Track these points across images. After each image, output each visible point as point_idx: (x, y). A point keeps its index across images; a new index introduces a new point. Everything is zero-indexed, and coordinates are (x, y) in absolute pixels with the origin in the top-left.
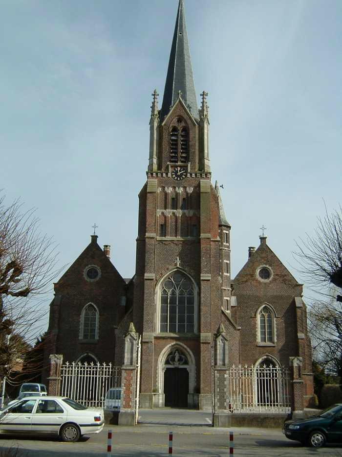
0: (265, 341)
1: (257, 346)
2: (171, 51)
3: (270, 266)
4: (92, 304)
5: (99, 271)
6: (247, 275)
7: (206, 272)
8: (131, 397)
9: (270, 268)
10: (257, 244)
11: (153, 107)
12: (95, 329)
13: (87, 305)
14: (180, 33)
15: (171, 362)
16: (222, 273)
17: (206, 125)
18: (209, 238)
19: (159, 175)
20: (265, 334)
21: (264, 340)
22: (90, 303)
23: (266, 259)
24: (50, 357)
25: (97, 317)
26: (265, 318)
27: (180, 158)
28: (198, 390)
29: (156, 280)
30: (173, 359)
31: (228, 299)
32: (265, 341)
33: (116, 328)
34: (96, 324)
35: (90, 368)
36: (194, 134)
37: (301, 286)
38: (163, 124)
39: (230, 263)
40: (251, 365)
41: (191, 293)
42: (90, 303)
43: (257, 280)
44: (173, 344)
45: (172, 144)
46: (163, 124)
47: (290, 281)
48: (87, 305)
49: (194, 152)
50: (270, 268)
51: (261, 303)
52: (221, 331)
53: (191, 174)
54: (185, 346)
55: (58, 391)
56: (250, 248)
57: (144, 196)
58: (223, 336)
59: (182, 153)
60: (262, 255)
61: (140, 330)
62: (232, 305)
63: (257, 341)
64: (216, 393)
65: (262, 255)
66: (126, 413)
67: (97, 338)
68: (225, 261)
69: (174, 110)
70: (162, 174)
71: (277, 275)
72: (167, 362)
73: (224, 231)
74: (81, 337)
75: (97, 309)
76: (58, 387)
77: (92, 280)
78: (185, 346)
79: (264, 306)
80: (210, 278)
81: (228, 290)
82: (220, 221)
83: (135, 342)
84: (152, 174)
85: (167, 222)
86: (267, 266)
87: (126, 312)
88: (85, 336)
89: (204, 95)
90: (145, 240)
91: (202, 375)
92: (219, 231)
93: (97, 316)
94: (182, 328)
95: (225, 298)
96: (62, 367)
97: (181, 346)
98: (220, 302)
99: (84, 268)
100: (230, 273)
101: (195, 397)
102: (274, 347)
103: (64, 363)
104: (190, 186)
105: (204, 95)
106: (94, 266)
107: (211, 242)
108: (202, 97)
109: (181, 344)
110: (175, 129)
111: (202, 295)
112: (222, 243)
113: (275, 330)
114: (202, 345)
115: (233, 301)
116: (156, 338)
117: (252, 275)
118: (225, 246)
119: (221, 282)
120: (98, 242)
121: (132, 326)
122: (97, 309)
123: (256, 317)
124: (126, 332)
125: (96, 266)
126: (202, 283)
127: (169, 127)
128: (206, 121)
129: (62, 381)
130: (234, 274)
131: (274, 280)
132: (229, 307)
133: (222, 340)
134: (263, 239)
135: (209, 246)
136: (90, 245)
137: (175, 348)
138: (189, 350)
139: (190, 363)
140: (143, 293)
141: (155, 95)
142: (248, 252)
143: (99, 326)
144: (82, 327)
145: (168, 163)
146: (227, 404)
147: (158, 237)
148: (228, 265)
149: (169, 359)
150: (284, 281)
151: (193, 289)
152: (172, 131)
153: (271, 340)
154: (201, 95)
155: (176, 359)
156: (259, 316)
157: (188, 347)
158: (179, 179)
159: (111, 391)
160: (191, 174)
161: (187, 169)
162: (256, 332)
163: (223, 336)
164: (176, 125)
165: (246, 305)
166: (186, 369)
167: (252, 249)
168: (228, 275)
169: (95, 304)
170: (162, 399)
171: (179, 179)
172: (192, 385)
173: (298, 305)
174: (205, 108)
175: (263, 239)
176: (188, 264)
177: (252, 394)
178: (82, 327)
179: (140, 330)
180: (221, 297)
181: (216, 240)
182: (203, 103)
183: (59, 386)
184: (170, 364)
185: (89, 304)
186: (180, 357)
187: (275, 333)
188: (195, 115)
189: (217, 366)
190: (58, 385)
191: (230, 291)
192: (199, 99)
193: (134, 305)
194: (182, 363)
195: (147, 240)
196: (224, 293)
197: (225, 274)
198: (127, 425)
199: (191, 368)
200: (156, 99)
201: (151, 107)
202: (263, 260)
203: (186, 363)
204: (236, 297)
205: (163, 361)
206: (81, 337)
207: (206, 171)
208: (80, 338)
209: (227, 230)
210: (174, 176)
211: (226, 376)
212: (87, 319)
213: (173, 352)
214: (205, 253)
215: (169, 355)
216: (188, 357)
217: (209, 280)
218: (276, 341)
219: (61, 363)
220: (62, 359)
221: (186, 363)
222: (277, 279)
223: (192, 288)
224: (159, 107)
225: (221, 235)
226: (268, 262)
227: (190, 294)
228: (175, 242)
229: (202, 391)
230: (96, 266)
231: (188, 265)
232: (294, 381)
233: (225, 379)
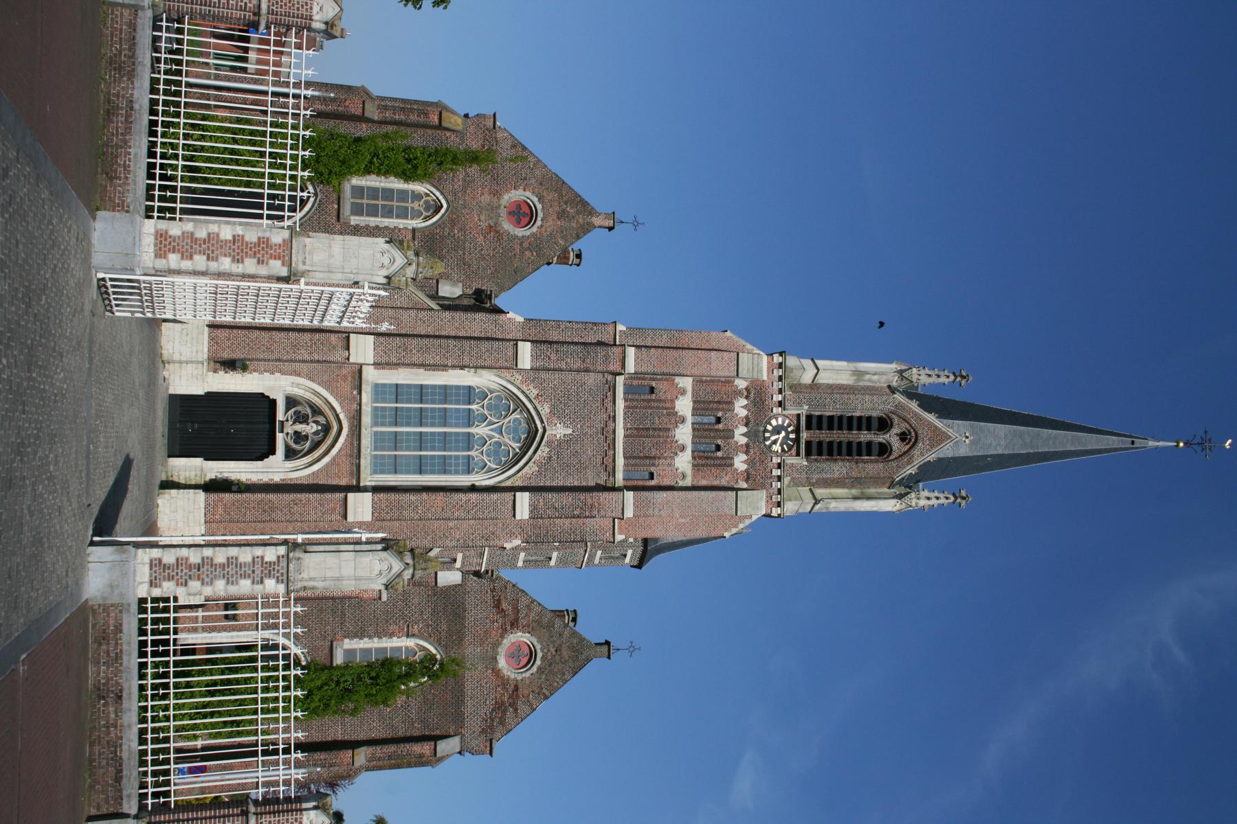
3: (539, 668)
4: (443, 211)
6: (516, 610)
7: (533, 508)
9: (535, 669)
10: (590, 630)
12: (377, 216)
13: (441, 198)
15: (293, 410)
22: (445, 206)
30: (301, 419)
31: (458, 564)
35: (293, 168)
40: (303, 627)
42: (445, 206)
43: (502, 637)
47: (502, 722)
48: (441, 198)
63: (346, 641)
69: (930, 424)
71: (516, 688)
72: (291, 402)
80: (518, 517)
86: (538, 662)
95: (460, 557)
98: (454, 543)
109: (342, 440)
122: (428, 223)
123: (408, 636)
136: (116, 522)
149: (299, 408)
150: (500, 707)
155: (299, 427)
162: (370, 637)
166: (274, 453)
168: (520, 564)
173: (442, 746)
177: (204, 629)
184: (287, 410)
185: (443, 202)
186: (306, 437)
196: (472, 552)
199: (275, 468)
202: (553, 650)
203: (290, 454)
222: (505, 688)
223: (491, 470)
228: (611, 423)
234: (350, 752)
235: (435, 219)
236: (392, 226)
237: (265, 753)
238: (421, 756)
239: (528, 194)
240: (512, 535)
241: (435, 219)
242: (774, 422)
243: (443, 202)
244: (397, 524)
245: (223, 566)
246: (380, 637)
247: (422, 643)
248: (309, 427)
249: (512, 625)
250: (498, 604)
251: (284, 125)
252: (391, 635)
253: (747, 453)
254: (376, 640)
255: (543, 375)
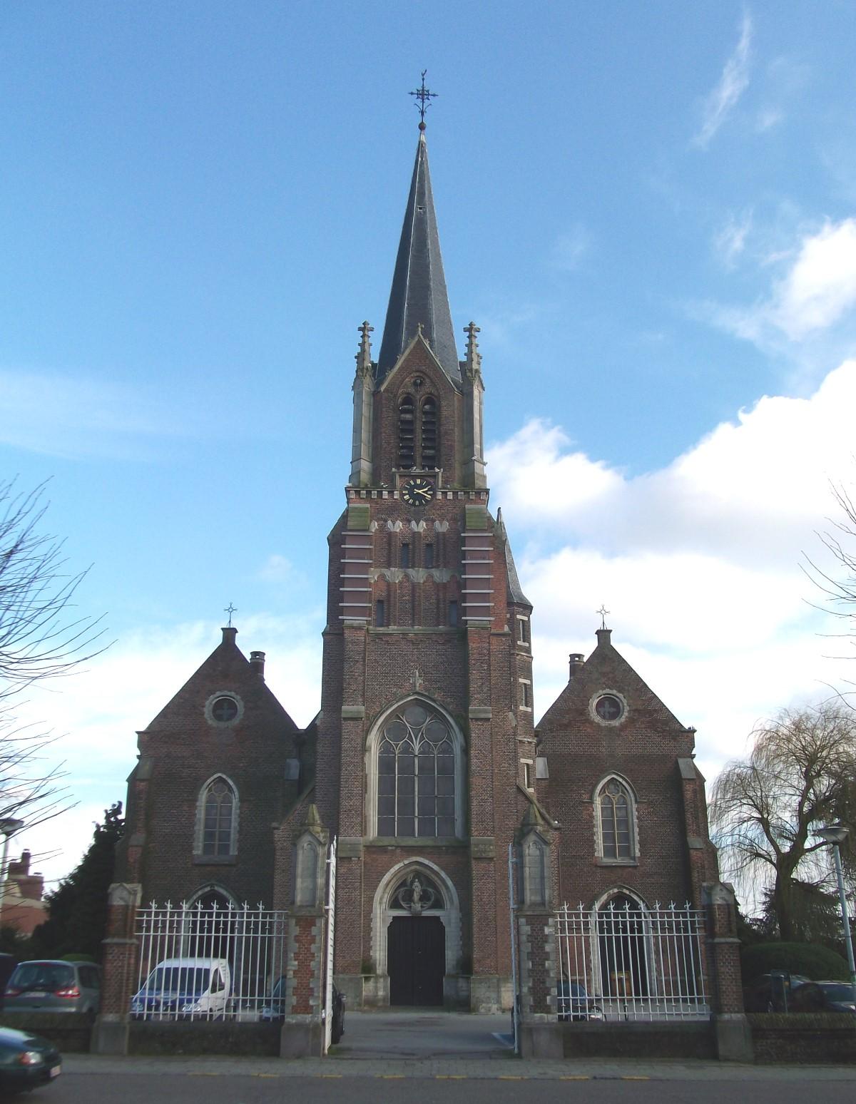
0: (616, 858)
1: (596, 866)
2: (407, 213)
3: (619, 692)
4: (224, 776)
5: (240, 705)
8: (311, 986)
9: (620, 695)
10: (588, 648)
11: (361, 357)
13: (212, 778)
14: (420, 208)
15: (402, 903)
16: (517, 707)
17: (476, 392)
18: (487, 629)
19: (374, 494)
20: (615, 840)
21: (609, 852)
22: (219, 775)
23: (611, 675)
24: (109, 890)
25: (234, 805)
26: (612, 805)
27: (419, 460)
28: (466, 967)
29: (368, 718)
30: (409, 897)
31: (530, 762)
32: (616, 858)
33: (277, 829)
34: (233, 820)
36: (450, 408)
37: (689, 734)
38: (382, 389)
39: (531, 685)
41: (448, 749)
42: (219, 775)
44: (406, 862)
45: (403, 431)
46: (382, 389)
48: (212, 778)
49: (452, 447)
50: (620, 695)
51: (604, 772)
52: (533, 822)
53: (445, 494)
54: (435, 867)
55: (128, 973)
56: (572, 656)
57: (337, 540)
58: (538, 835)
59: (424, 448)
60: (603, 670)
61: (333, 827)
62: (538, 776)
63: (596, 854)
64: (524, 974)
65: (603, 670)
66: (299, 1026)
67: (233, 851)
68: (522, 680)
70: (380, 494)
71: (636, 710)
72: (395, 904)
73: (519, 617)
74: (198, 851)
75: (234, 787)
76: (129, 964)
77: (222, 725)
78: (435, 867)
79: (609, 778)
80: (490, 716)
81: (530, 743)
82: (509, 595)
83: (321, 851)
84: (358, 493)
85: (392, 594)
86: (614, 692)
87: (300, 792)
88: (208, 849)
89: (471, 330)
90: (342, 634)
91: (475, 930)
92: (508, 616)
93: (235, 801)
94: (426, 829)
95: (523, 761)
96: (141, 914)
97: (426, 866)
99: (207, 699)
100: (532, 706)
101: (462, 983)
102: (635, 867)
103: (145, 904)
104: (442, 518)
105: (471, 330)
106: (229, 694)
107: (494, 640)
108: (468, 334)
109: (426, 862)
110: (408, 400)
111: (473, 752)
112: (514, 642)
113: (636, 830)
114: (473, 862)
115: (541, 766)
116: (370, 848)
117: (582, 712)
118: (522, 649)
119: (514, 724)
120: (238, 643)
121: (315, 812)
122: (234, 787)
124: (303, 828)
125: (233, 694)
126: (473, 725)
127: (395, 396)
128: (476, 384)
129: (138, 947)
130: (540, 708)
131: (631, 721)
132: (531, 781)
133: (535, 843)
134: (603, 635)
135: (486, 645)
137: (412, 871)
138: (443, 874)
139: (448, 905)
140: (340, 748)
141: (364, 329)
142: (568, 666)
143: (240, 824)
144: (200, 829)
145: (394, 470)
146: (551, 1000)
147: (371, 627)
148: (528, 690)
149: (400, 897)
151: (452, 742)
152: (403, 404)
153: (627, 851)
154: (465, 330)
155: (416, 897)
156: (598, 801)
157: (442, 868)
158: (417, 503)
159: (160, 970)
160: (445, 494)
161: (436, 483)
162: (593, 834)
163: (538, 835)
164: (411, 390)
165: (567, 783)
166: (438, 918)
167: (577, 659)
168: (529, 709)
169: (230, 776)
170: (385, 987)
171: (417, 503)
172: (451, 955)
174: (474, 356)
175: (603, 635)
176: (439, 685)
178: (200, 829)
179: (333, 827)
180: (515, 759)
181: (500, 632)
182: (470, 346)
183: (132, 961)
185: (216, 776)
186: (424, 891)
187: (637, 838)
188: (453, 375)
189: (526, 907)
190: (130, 958)
191: (533, 745)
192: (460, 340)
193: (319, 776)
194: (430, 903)
195: (347, 633)
196: (520, 750)
197: (522, 708)
198: (300, 1056)
199: (449, 916)
200: (366, 338)
201: (359, 345)
204: (546, 759)
205: (384, 900)
206: (198, 851)
207: (477, 486)
208: (195, 852)
209: (524, 615)
210: (406, 497)
211: (547, 930)
212: (215, 805)
213: (409, 880)
214: (477, 660)
215: (399, 887)
216: (443, 891)
217: (488, 719)
218: (638, 854)
219: (138, 902)
220: (139, 896)
221: (438, 904)
224: (374, 355)
225: (512, 622)
226: (614, 683)
227: (444, 752)
229: (476, 967)
230: (233, 694)
231: (439, 688)
232: (717, 940)
233: (545, 939)
234: (692, 851)
235: (231, 783)
236: (238, 820)
237: (640, 931)
238: (695, 792)
239: (207, 703)
240: (505, 719)
241: (231, 783)
242: (406, 497)
243: (216, 776)
244: (496, 816)
245: (308, 949)
246: (593, 826)
247: (598, 791)
248: (417, 889)
249: (581, 714)
250: (566, 727)
251: (256, 923)
252: (592, 817)
253: (433, 521)
254: (595, 830)
255: (368, 694)
